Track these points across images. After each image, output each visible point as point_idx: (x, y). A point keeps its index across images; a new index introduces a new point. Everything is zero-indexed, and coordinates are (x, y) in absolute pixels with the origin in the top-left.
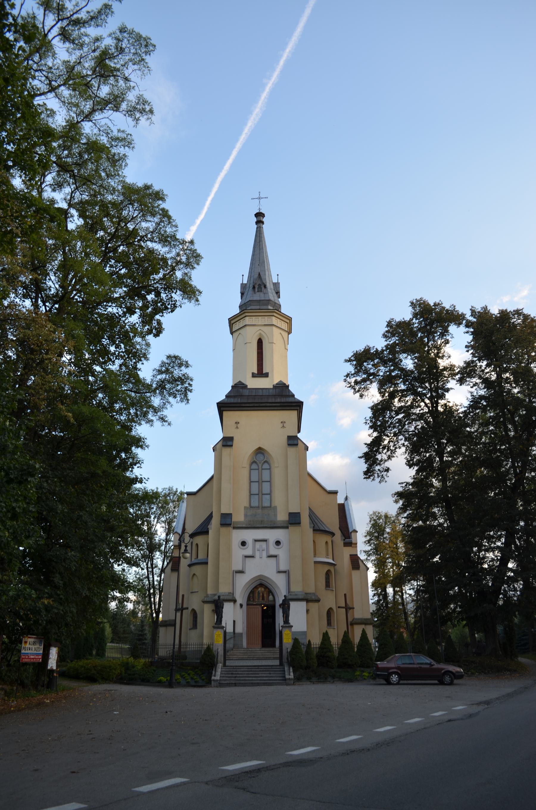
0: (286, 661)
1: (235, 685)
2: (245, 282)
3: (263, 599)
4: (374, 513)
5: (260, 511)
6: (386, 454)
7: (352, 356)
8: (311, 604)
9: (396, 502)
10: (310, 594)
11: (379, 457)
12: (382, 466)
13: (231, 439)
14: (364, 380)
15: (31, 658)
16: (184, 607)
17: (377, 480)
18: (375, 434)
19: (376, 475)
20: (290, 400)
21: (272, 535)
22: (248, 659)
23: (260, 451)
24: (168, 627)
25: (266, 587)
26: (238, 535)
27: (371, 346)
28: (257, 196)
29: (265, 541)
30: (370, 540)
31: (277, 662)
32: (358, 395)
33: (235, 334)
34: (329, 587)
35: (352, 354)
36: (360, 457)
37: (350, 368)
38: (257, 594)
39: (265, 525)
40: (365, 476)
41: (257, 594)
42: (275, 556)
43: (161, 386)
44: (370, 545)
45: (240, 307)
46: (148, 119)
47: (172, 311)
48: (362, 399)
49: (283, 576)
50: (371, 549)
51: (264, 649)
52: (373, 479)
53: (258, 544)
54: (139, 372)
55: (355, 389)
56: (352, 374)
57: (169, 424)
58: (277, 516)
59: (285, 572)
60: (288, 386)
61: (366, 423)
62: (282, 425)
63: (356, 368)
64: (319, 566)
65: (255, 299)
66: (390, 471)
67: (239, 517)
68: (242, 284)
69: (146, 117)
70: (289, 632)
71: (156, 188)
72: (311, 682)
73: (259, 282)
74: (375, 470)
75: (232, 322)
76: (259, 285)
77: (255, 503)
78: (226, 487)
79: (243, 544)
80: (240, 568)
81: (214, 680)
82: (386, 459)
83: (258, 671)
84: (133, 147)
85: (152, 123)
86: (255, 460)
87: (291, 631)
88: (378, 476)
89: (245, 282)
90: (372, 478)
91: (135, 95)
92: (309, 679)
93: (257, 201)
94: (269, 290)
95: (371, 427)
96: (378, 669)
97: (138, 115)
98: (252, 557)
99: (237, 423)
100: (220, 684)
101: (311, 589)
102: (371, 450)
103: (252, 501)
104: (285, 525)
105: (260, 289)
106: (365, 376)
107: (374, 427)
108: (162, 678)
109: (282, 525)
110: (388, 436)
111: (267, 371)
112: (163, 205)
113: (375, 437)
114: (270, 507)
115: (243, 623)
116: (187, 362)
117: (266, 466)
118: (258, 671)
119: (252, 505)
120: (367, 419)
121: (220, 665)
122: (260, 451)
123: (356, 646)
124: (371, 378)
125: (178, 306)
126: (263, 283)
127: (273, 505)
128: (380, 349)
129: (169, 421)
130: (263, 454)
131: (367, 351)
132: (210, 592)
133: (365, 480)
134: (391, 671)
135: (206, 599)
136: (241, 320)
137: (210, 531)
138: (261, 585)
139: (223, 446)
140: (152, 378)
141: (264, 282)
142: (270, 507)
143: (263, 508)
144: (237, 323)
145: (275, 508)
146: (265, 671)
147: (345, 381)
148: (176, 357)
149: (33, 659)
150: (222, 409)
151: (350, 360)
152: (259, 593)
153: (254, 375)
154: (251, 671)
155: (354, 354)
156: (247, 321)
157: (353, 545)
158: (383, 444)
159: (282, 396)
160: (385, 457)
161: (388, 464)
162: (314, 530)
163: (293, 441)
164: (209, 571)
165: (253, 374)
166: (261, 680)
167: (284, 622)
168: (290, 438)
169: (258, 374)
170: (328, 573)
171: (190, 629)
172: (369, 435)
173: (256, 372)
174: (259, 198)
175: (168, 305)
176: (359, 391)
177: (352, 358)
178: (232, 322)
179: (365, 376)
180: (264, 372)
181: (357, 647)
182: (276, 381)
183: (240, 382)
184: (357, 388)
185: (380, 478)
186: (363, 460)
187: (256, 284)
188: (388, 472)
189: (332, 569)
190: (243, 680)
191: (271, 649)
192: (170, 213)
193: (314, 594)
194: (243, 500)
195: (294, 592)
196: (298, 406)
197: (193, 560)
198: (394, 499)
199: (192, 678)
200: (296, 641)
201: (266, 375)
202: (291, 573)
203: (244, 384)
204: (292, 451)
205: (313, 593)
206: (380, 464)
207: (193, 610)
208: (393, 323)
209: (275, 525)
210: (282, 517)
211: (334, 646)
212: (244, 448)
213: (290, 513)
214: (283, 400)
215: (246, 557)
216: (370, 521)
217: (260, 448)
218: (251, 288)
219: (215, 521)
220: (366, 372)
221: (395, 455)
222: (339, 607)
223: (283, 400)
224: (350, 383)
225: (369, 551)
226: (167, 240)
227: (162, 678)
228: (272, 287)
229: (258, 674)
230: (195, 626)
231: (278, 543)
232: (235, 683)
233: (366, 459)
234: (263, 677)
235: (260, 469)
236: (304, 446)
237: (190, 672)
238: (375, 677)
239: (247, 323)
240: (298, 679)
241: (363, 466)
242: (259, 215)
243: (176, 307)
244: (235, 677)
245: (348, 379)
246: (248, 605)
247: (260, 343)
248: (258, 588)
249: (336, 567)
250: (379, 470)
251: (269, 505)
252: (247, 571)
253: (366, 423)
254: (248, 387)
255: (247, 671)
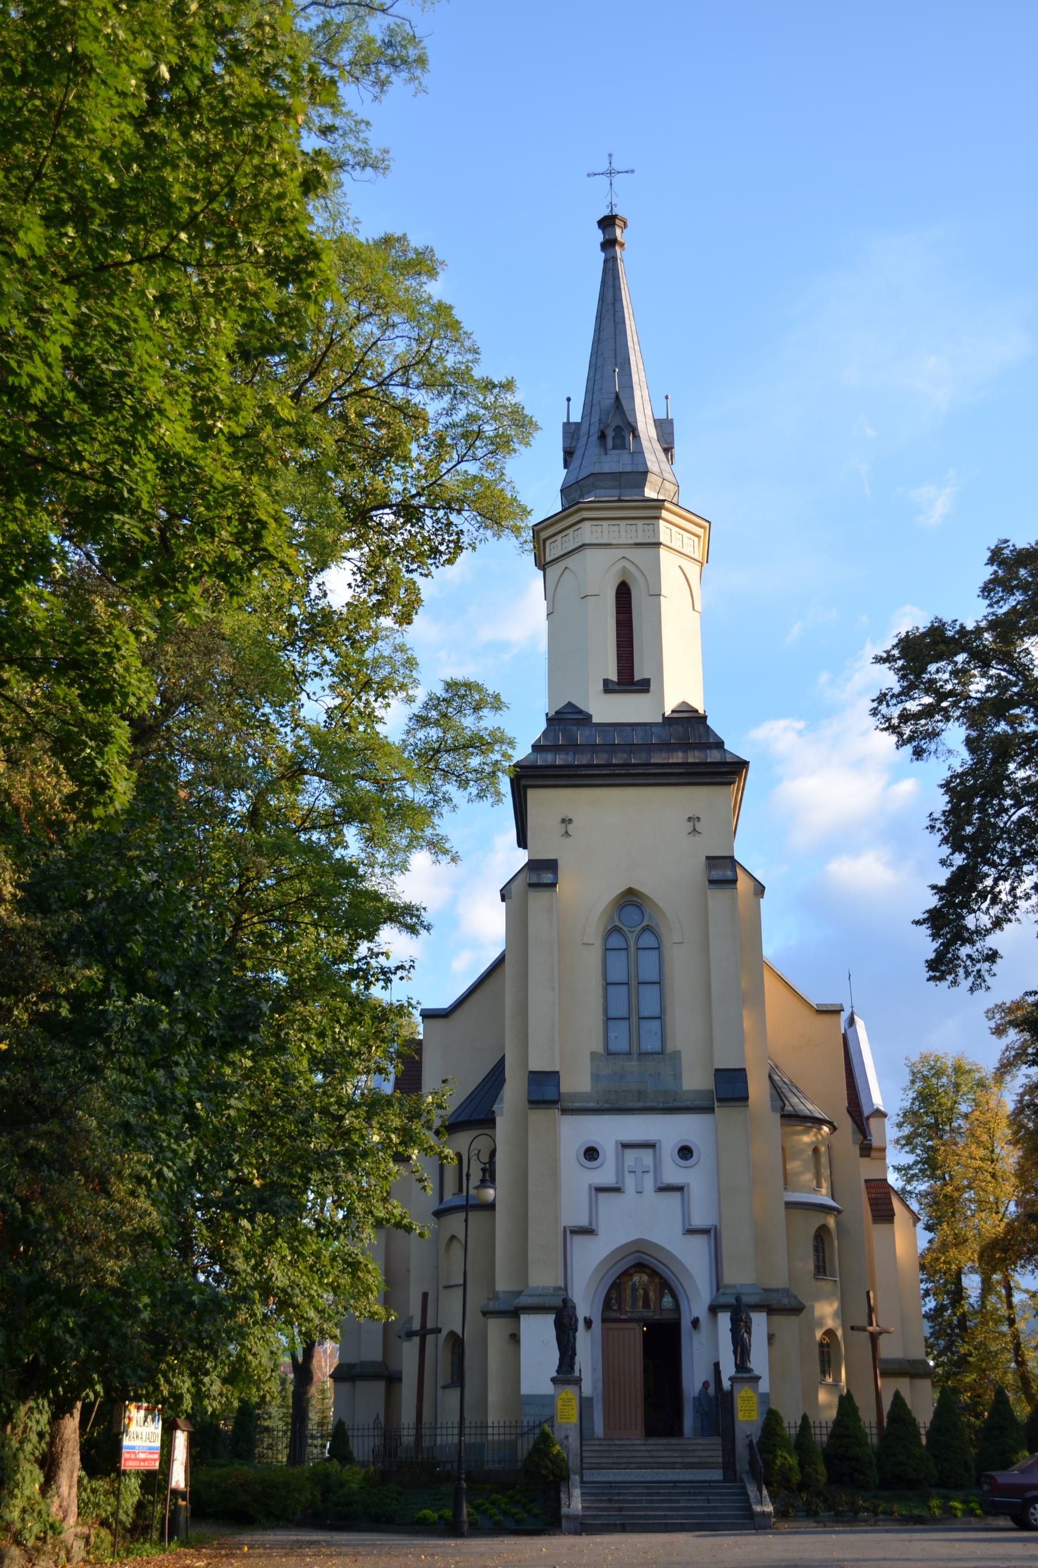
0: (747, 1467)
1: (623, 1529)
2: (576, 417)
3: (646, 1304)
4: (924, 1059)
5: (633, 1064)
6: (987, 912)
7: (894, 647)
8: (778, 1319)
9: (999, 1031)
10: (777, 1290)
11: (970, 921)
12: (978, 945)
13: (551, 865)
14: (928, 712)
15: (140, 1460)
16: (430, 1325)
17: (966, 984)
18: (959, 859)
19: (961, 971)
20: (714, 756)
21: (669, 1130)
22: (628, 1466)
23: (630, 900)
24: (361, 1385)
25: (654, 1273)
26: (575, 1132)
27: (947, 619)
28: (604, 167)
29: (651, 1146)
30: (914, 1135)
31: (717, 1475)
32: (909, 749)
33: (554, 571)
34: (825, 1274)
35: (895, 641)
36: (917, 923)
37: (889, 679)
38: (628, 1292)
39: (649, 1104)
40: (932, 973)
41: (628, 1292)
42: (679, 1189)
43: (430, 754)
44: (912, 1151)
45: (565, 491)
46: (413, 79)
47: (450, 561)
48: (920, 762)
49: (700, 1245)
50: (916, 1163)
51: (653, 1441)
52: (954, 983)
53: (631, 1155)
54: (379, 727)
55: (901, 735)
56: (893, 696)
57: (453, 860)
58: (680, 1078)
59: (705, 1231)
60: (705, 718)
61: (933, 827)
62: (689, 827)
63: (903, 677)
64: (798, 1214)
65: (607, 470)
66: (998, 960)
67: (577, 1081)
68: (567, 425)
69: (404, 75)
70: (750, 1393)
71: (416, 242)
72: (818, 1522)
73: (618, 422)
74: (958, 958)
75: (544, 535)
76: (618, 429)
77: (620, 1043)
78: (540, 995)
79: (591, 1153)
80: (583, 1221)
81: (567, 1516)
82: (989, 926)
83: (676, 1494)
84: (387, 168)
85: (422, 90)
86: (618, 923)
87: (755, 1389)
88: (967, 974)
89: (576, 417)
90: (950, 978)
91: (385, 26)
92: (810, 1514)
93: (604, 180)
94: (645, 443)
95: (945, 840)
96: (997, 1488)
97: (385, 71)
98: (617, 1190)
99: (566, 821)
100: (584, 1527)
101: (779, 1280)
102: (950, 904)
103: (612, 1035)
104: (705, 1103)
105: (619, 442)
106: (928, 700)
107: (955, 841)
108: (427, 1512)
109: (697, 1103)
110: (994, 865)
111: (646, 676)
112: (435, 289)
113: (960, 868)
114: (662, 1052)
115: (594, 1370)
116: (497, 697)
117: (648, 940)
118: (676, 1494)
119: (613, 1047)
120: (935, 816)
121: (575, 1478)
122: (630, 900)
123: (923, 1431)
124: (944, 704)
125: (465, 545)
126: (629, 423)
127: (670, 1048)
128: (970, 626)
129: (454, 850)
130: (639, 907)
131: (936, 631)
132: (502, 1285)
133: (932, 983)
134: (1030, 1494)
135: (492, 1306)
136: (570, 531)
137: (499, 1120)
138: (640, 1267)
139: (531, 885)
140: (404, 737)
141: (630, 420)
142: (662, 1052)
143: (643, 1055)
144: (558, 537)
145: (676, 1055)
146: (695, 1494)
147: (875, 712)
148: (468, 686)
149: (144, 1460)
150: (523, 782)
151: (888, 659)
152: (634, 1289)
153: (609, 687)
154: (658, 1494)
155: (901, 640)
156: (588, 532)
157: (873, 1154)
158: (980, 887)
159: (686, 746)
160: (985, 921)
161: (993, 941)
162: (782, 1116)
163: (723, 871)
164: (497, 1229)
165: (606, 682)
166: (687, 1517)
167: (736, 1365)
168: (713, 861)
169: (619, 683)
170: (821, 1235)
171: (444, 1387)
172: (943, 862)
173: (613, 677)
174: (610, 173)
175: (441, 544)
176: (911, 739)
177: (896, 652)
178: (544, 535)
179: (928, 700)
180: (637, 677)
181: (928, 1434)
182: (669, 706)
183: (570, 704)
184: (907, 731)
185: (971, 979)
186: (925, 931)
187: (608, 426)
188: (994, 962)
189: (831, 1222)
190: (640, 1517)
191: (674, 1441)
192: (458, 314)
193: (786, 1292)
194: (589, 1035)
195: (735, 1286)
196: (730, 771)
197: (448, 1197)
198: (992, 1024)
199: (505, 1513)
200: (772, 1419)
201: (644, 686)
202: (725, 1235)
203: (580, 712)
204: (718, 897)
205: (784, 1290)
206: (973, 943)
207: (452, 1334)
208: (1007, 551)
209: (676, 1104)
210: (695, 1079)
211: (868, 1431)
212: (586, 892)
213: (718, 1071)
214: (694, 758)
215: (600, 1190)
216: (913, 1082)
217: (630, 891)
218: (594, 438)
219: (513, 1092)
220: (931, 687)
221: (1013, 917)
222: (852, 1328)
223: (694, 757)
224: (889, 720)
225: (910, 1167)
226: (450, 383)
227: (427, 1512)
228: (653, 433)
229: (678, 1501)
230: (458, 1378)
231: (685, 1152)
232: (623, 1525)
233: (933, 927)
234: (692, 1508)
235: (632, 949)
236: (752, 884)
237: (495, 1496)
238: (992, 1509)
239: (587, 541)
240: (782, 1514)
241: (927, 946)
242: (608, 223)
243: (461, 548)
244: (620, 1509)
245: (883, 708)
246: (604, 1320)
247: (624, 594)
248: (631, 1275)
249: (841, 1216)
250: (969, 956)
251: (657, 1048)
252: (602, 1228)
253: (933, 827)
254: (595, 720)
255: (649, 1494)
